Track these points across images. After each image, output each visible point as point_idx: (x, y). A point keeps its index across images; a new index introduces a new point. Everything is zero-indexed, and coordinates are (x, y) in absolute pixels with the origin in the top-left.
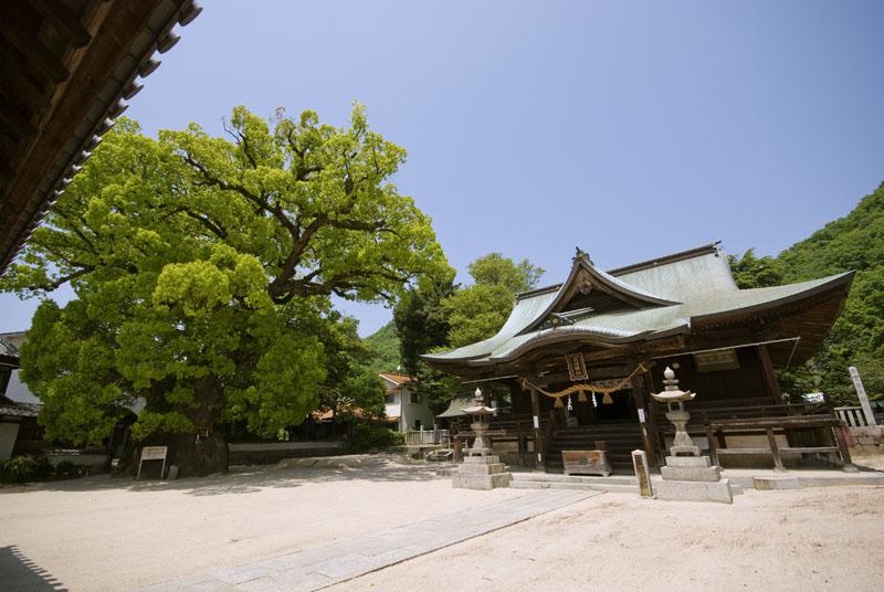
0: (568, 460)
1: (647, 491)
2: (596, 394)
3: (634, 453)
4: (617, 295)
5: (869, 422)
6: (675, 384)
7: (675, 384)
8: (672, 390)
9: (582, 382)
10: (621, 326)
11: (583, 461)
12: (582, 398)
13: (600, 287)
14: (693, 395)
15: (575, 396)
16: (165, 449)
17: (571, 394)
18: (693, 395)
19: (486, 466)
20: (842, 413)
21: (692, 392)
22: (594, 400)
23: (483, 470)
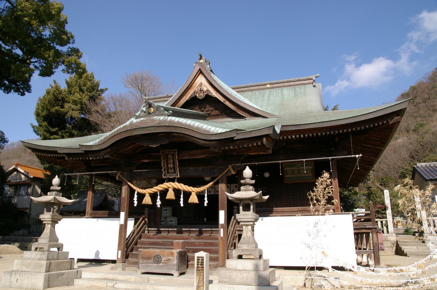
0: (143, 258)
1: (327, 256)
2: (138, 194)
3: (197, 255)
4: (227, 103)
5: (389, 231)
6: (251, 185)
7: (251, 185)
8: (246, 190)
9: (173, 180)
10: (215, 128)
11: (157, 259)
12: (171, 195)
13: (214, 94)
14: (266, 197)
15: (164, 193)
16: (152, 204)
17: (161, 191)
18: (266, 197)
19: (44, 263)
20: (379, 223)
21: (264, 194)
22: (182, 199)
23: (40, 266)
